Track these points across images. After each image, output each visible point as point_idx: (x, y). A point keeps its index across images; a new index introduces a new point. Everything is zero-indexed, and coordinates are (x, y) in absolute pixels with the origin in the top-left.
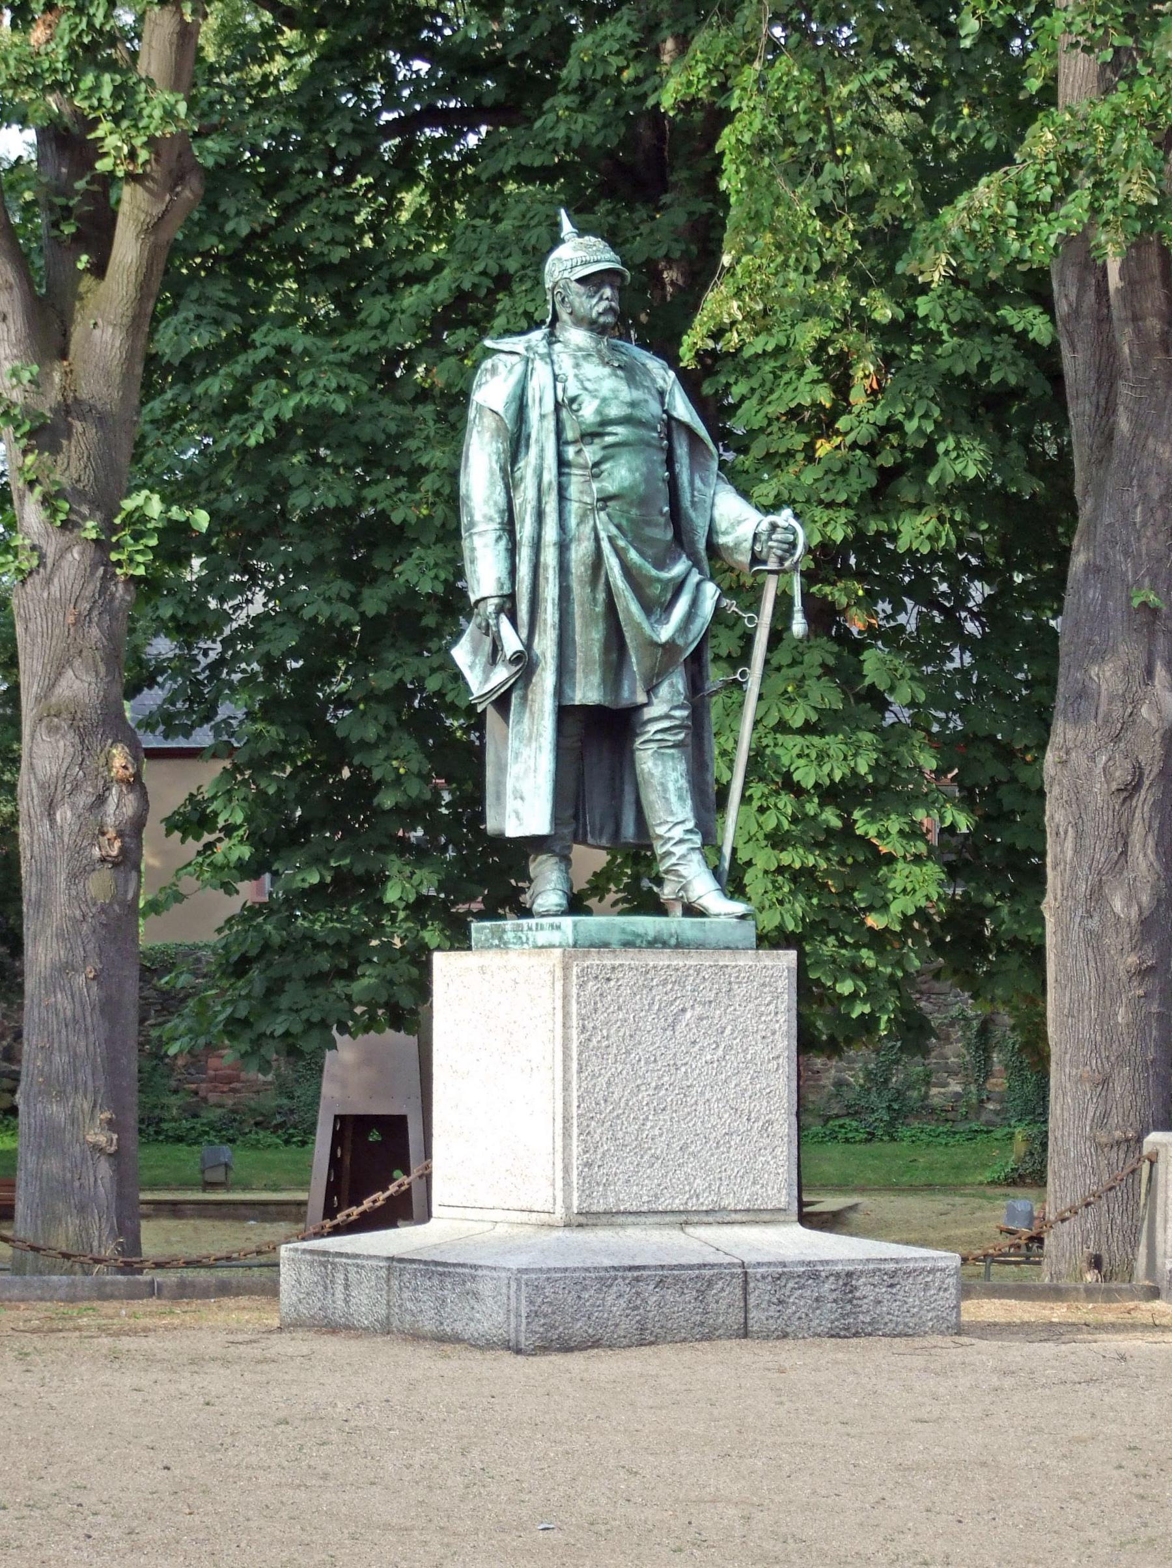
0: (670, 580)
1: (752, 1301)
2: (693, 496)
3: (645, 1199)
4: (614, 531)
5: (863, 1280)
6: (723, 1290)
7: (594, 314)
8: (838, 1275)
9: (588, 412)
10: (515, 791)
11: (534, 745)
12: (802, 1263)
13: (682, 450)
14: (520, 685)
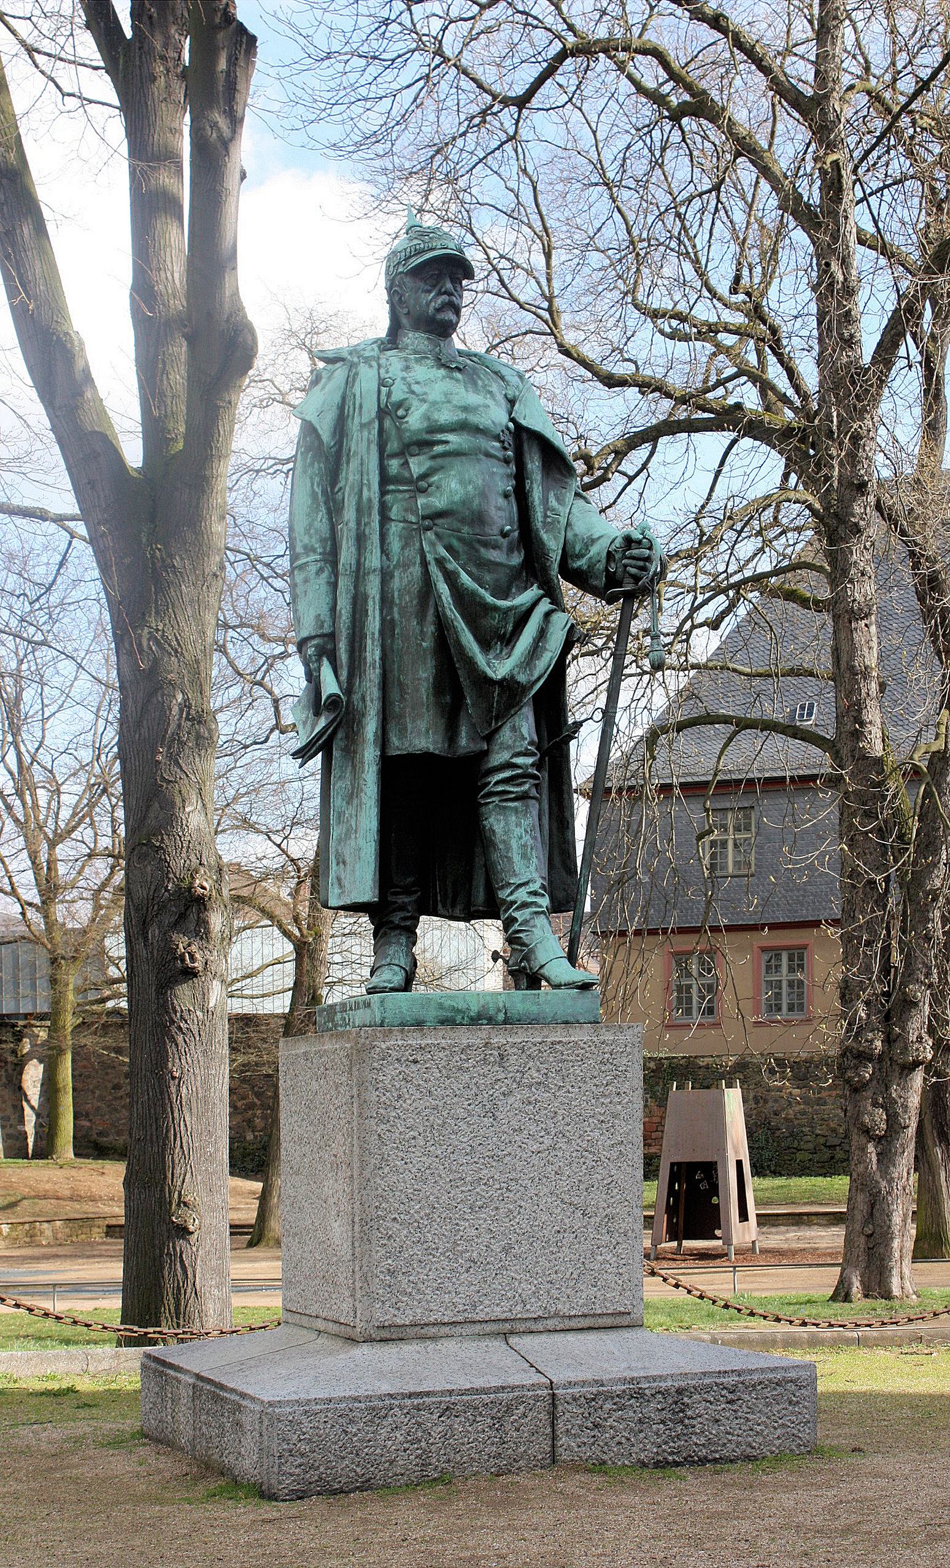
0: (510, 609)
1: (561, 1426)
2: (546, 516)
3: (461, 1307)
4: (443, 552)
5: (696, 1397)
6: (525, 1415)
7: (431, 310)
8: (665, 1393)
9: (415, 421)
10: (338, 855)
11: (355, 801)
12: (624, 1381)
13: (534, 464)
14: (340, 735)
